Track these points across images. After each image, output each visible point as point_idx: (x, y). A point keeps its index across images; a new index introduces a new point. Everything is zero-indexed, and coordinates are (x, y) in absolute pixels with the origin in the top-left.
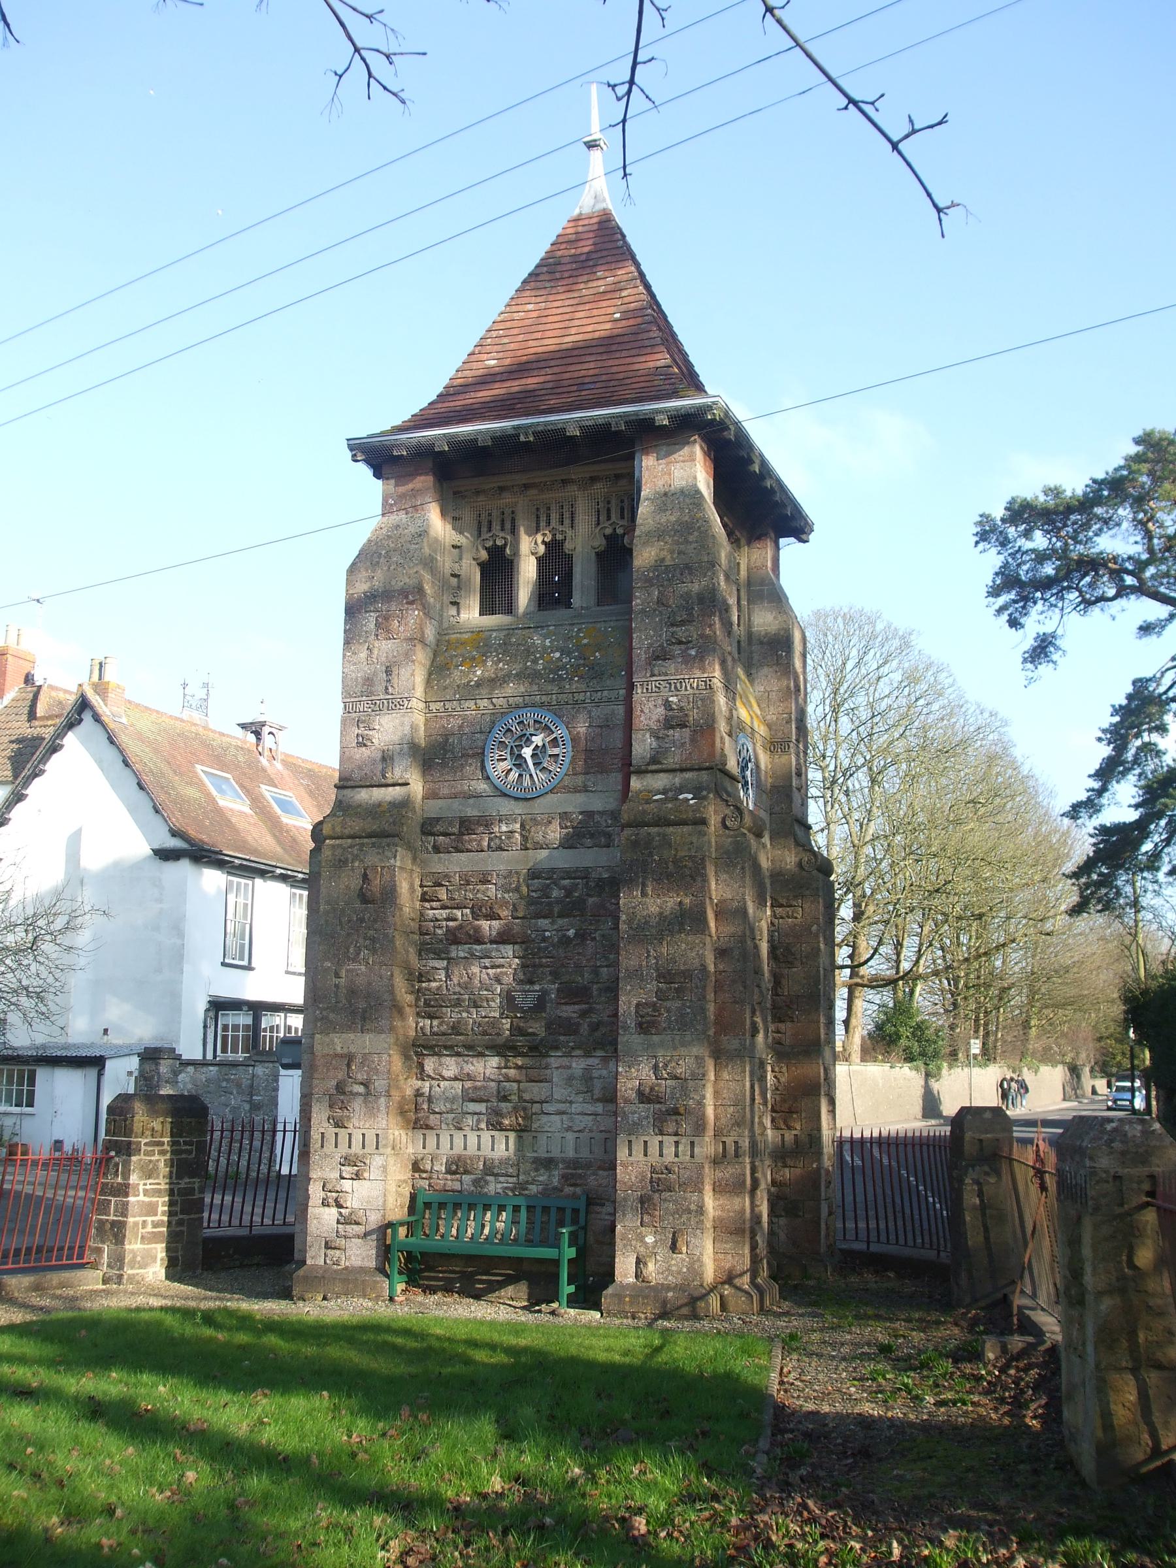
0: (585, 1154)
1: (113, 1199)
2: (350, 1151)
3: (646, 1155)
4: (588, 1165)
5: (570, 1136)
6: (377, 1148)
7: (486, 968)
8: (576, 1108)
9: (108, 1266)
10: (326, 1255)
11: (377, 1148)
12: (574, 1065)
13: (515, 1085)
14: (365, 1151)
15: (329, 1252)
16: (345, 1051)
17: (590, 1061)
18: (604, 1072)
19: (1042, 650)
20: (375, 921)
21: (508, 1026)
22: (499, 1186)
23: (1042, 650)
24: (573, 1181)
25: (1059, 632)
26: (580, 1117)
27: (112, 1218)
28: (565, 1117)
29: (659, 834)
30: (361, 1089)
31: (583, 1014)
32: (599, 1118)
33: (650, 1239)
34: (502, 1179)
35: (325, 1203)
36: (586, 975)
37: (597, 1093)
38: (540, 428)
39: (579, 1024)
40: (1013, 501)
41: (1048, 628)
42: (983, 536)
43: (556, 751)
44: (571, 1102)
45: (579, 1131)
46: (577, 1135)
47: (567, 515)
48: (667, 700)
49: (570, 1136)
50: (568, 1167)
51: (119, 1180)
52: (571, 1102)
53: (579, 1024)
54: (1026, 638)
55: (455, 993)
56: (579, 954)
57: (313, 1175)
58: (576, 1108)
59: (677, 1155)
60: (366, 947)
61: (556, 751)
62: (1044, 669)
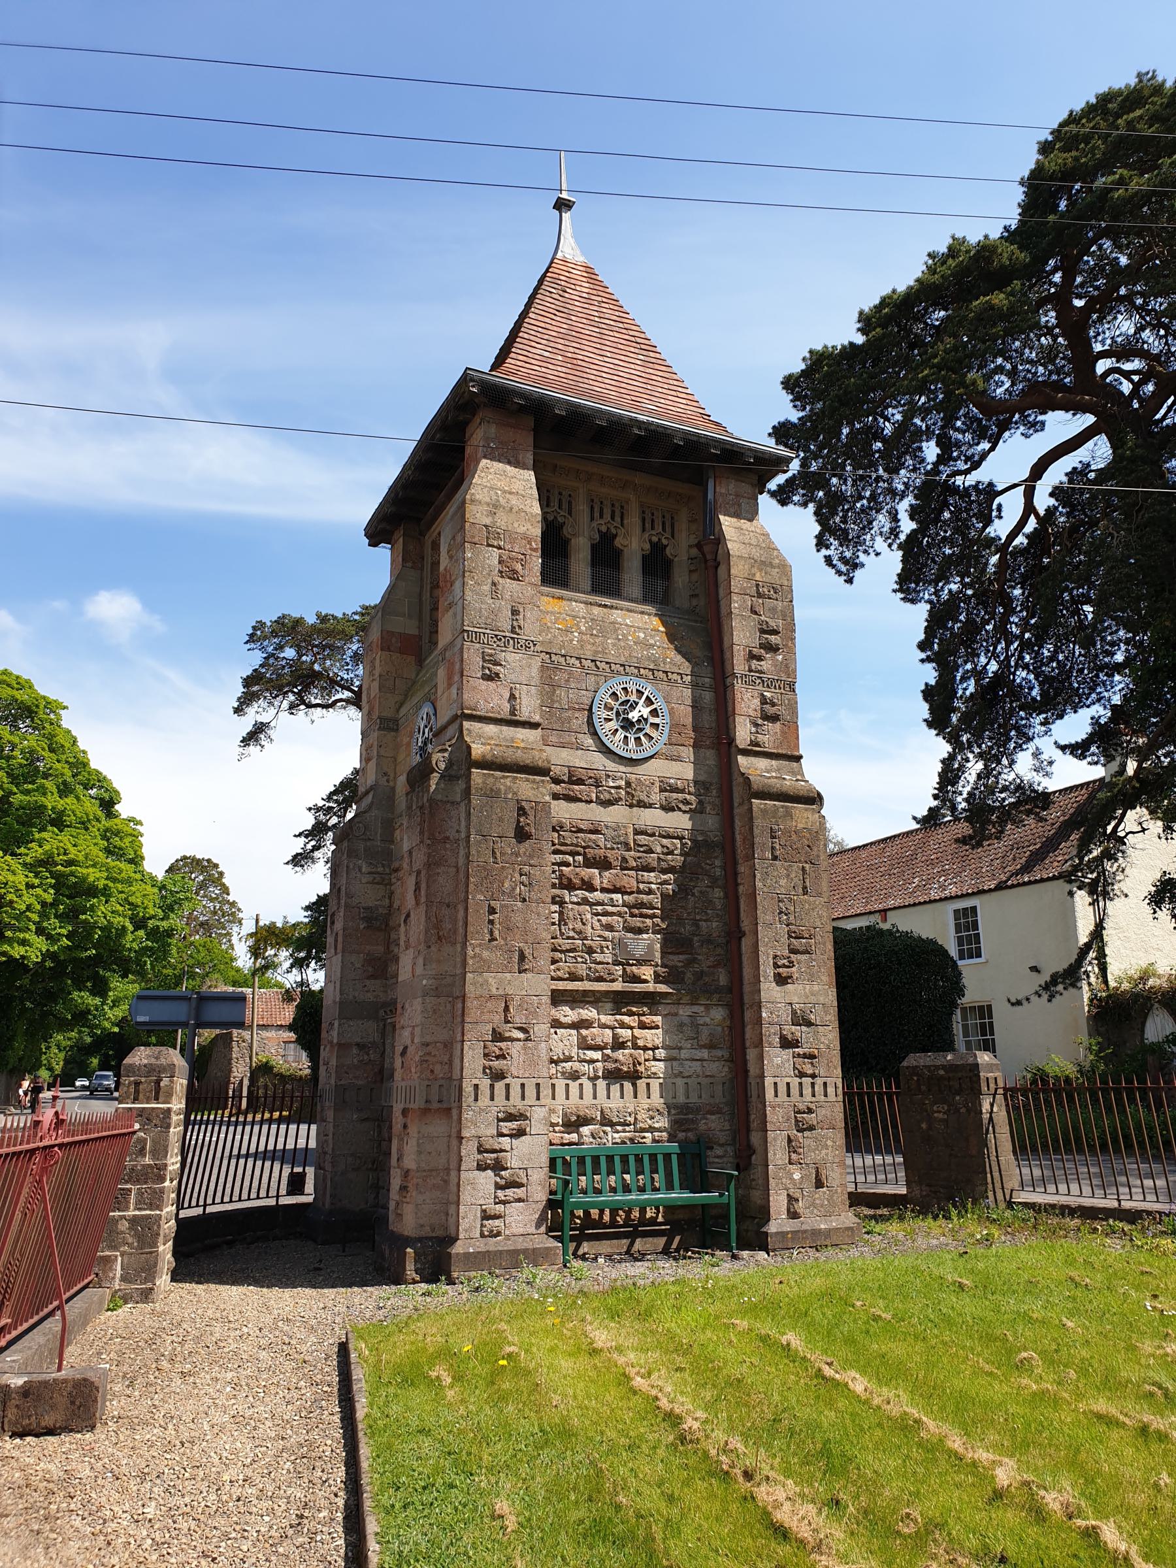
0: (694, 1099)
1: (134, 1188)
2: (509, 1104)
3: (789, 1095)
4: (698, 1110)
5: (680, 1082)
6: (538, 1098)
7: (597, 914)
8: (684, 1054)
9: (124, 1279)
10: (482, 1226)
11: (538, 1098)
12: (681, 1012)
13: (608, 1032)
14: (525, 1102)
15: (485, 1222)
16: (501, 992)
17: (696, 1009)
18: (708, 1020)
19: (255, 735)
20: (531, 857)
21: (620, 973)
22: (616, 1135)
23: (255, 735)
24: (687, 1126)
25: (272, 724)
26: (689, 1063)
27: (131, 1213)
28: (675, 1063)
29: (783, 807)
30: (521, 1035)
31: (689, 963)
32: (705, 1063)
33: (797, 1176)
34: (619, 1128)
35: (481, 1167)
36: (688, 927)
37: (704, 1038)
38: (652, 428)
39: (683, 973)
40: (302, 618)
41: (264, 718)
42: (252, 638)
43: (656, 720)
44: (680, 1048)
45: (689, 1077)
46: (685, 1080)
47: (618, 514)
48: (762, 695)
49: (680, 1082)
50: (678, 1114)
51: (148, 1160)
52: (680, 1048)
53: (683, 973)
54: (246, 724)
55: (568, 938)
56: (682, 907)
57: (466, 1133)
58: (684, 1054)
59: (814, 1095)
60: (522, 883)
61: (656, 720)
62: (253, 749)
